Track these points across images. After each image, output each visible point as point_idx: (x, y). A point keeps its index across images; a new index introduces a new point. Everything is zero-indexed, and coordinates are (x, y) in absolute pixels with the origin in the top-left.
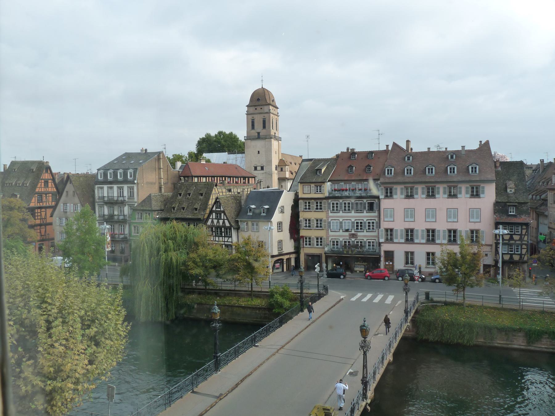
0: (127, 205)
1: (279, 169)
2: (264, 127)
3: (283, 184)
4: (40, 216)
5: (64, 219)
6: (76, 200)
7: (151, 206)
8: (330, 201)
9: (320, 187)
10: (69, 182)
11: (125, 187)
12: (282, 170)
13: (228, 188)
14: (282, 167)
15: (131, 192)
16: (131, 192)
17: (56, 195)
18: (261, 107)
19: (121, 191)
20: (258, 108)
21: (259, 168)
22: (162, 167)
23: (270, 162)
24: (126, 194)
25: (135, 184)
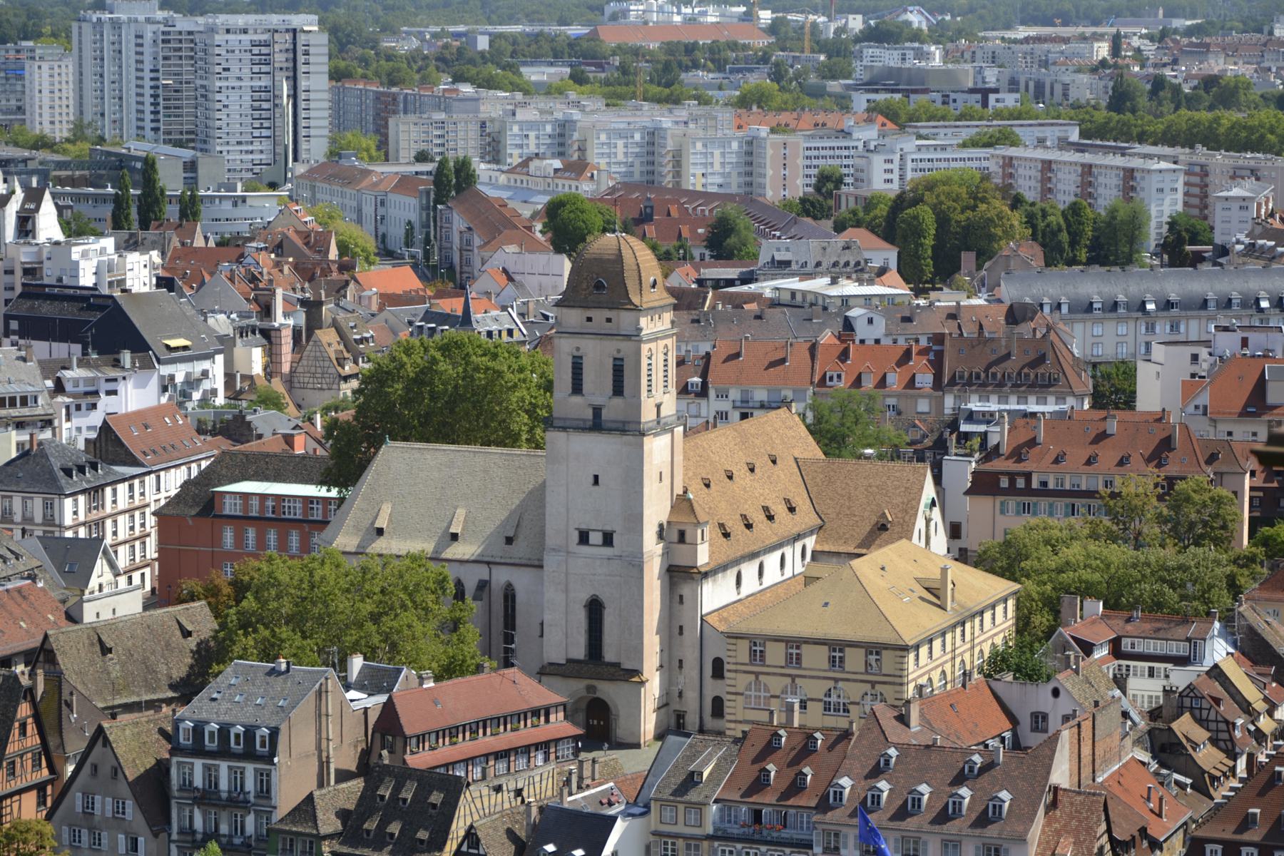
2: (618, 390)
3: (686, 590)
5: (85, 832)
7: (316, 826)
8: (716, 844)
11: (250, 768)
14: (682, 528)
15: (262, 781)
16: (262, 781)
20: (599, 315)
21: (596, 538)
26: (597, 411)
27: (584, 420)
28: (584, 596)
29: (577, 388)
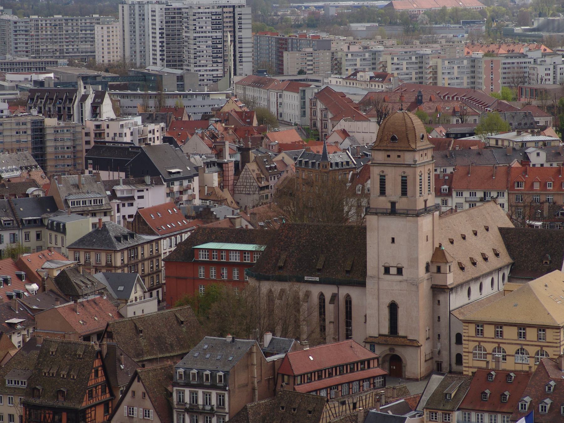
0: (215, 416)
1: (433, 269)
2: (404, 193)
3: (441, 298)
4: (90, 417)
6: (148, 404)
9: (449, 415)
10: (136, 380)
11: (214, 393)
12: (439, 270)
13: (342, 400)
14: (439, 265)
17: (105, 385)
18: (389, 153)
19: (208, 397)
20: (394, 155)
21: (393, 271)
22: (255, 363)
23: (414, 261)
24: (214, 402)
25: (226, 391)
26: (393, 204)
27: (387, 209)
28: (388, 301)
29: (383, 192)
